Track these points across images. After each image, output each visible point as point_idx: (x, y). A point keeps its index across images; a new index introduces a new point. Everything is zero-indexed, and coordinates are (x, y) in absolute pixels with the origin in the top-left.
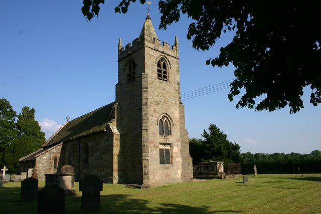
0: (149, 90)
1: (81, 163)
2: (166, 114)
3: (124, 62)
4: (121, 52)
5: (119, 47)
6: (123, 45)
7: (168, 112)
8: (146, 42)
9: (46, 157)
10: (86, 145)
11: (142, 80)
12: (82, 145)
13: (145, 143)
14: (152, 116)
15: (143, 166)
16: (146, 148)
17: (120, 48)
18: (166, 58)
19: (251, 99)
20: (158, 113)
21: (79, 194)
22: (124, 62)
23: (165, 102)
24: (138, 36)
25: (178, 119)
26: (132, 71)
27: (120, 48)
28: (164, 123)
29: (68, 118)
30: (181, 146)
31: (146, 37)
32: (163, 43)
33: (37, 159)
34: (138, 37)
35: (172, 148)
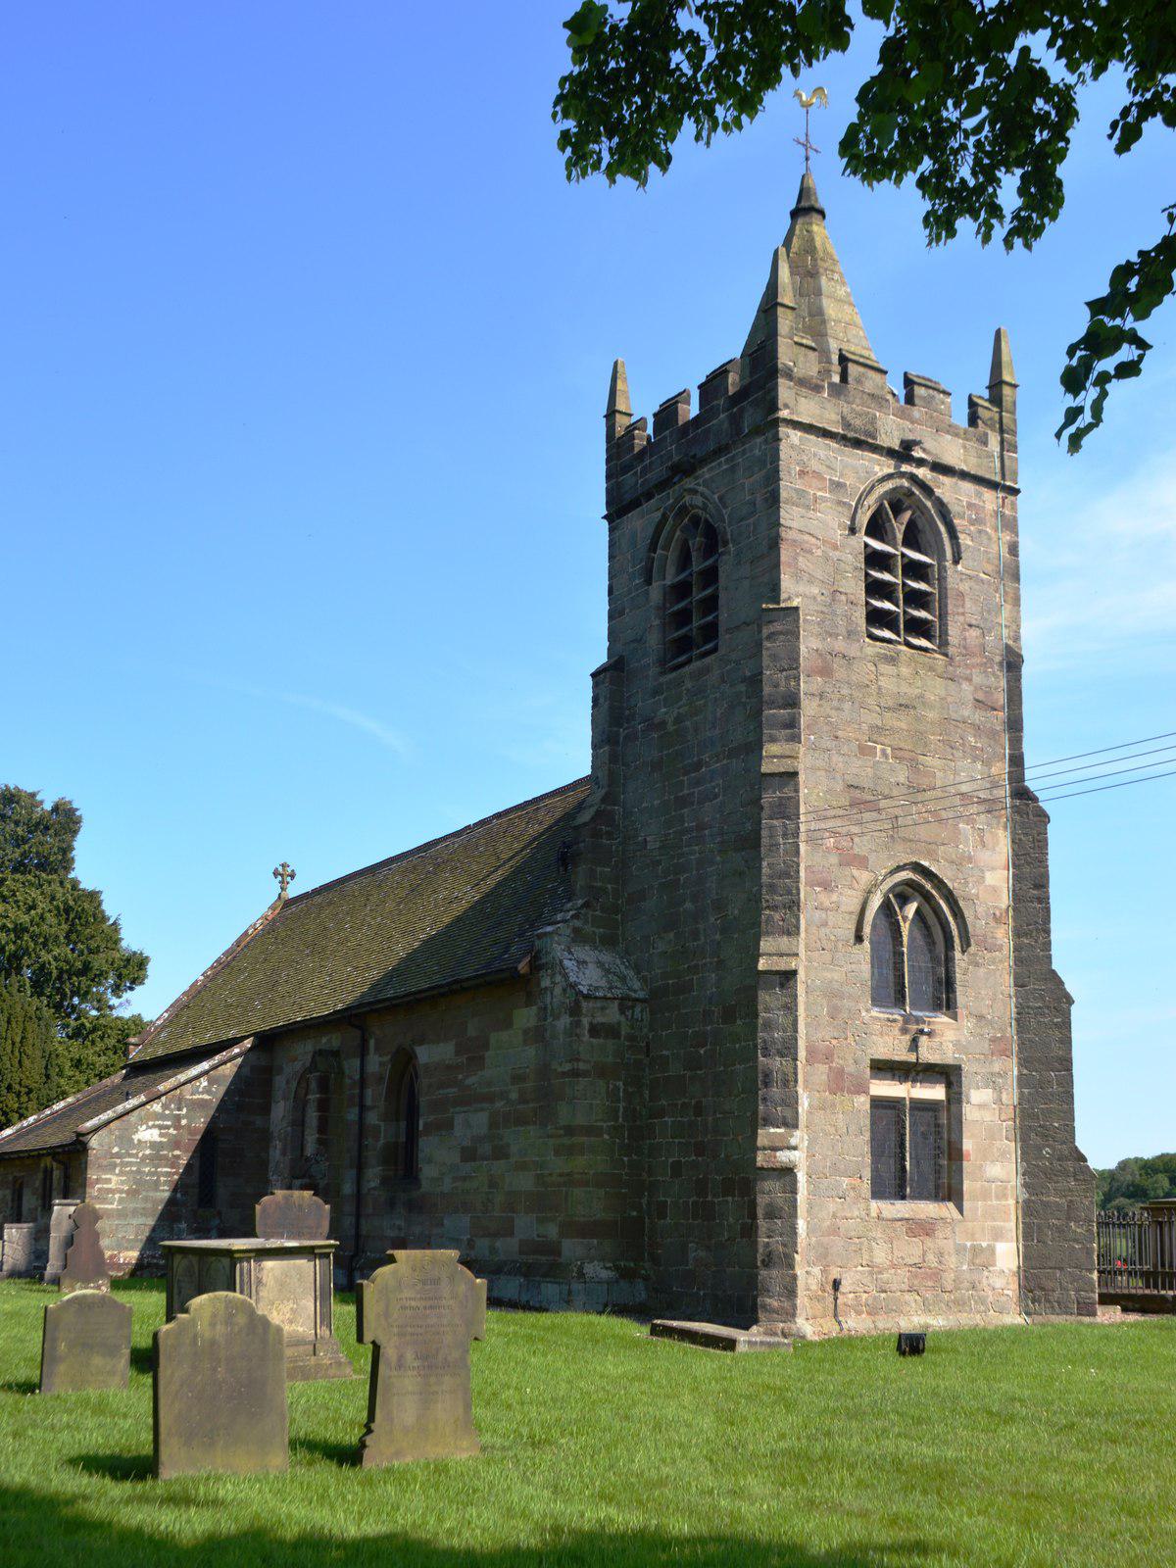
0: (808, 708)
1: (373, 1176)
2: (917, 867)
3: (641, 522)
4: (620, 450)
5: (611, 414)
6: (642, 406)
7: (931, 855)
8: (785, 391)
9: (148, 1134)
10: (404, 1064)
11: (759, 645)
12: (375, 1062)
13: (777, 1063)
14: (827, 886)
15: (760, 1212)
16: (776, 1091)
17: (622, 422)
18: (927, 490)
19: (994, 167)
20: (862, 862)
21: (1083, 21)
22: (641, 522)
23: (915, 790)
24: (732, 345)
25: (1005, 900)
26: (697, 565)
27: (622, 422)
28: (905, 928)
29: (284, 874)
30: (1022, 1081)
31: (785, 354)
32: (909, 382)
33: (94, 1142)
34: (737, 353)
35: (955, 1097)
